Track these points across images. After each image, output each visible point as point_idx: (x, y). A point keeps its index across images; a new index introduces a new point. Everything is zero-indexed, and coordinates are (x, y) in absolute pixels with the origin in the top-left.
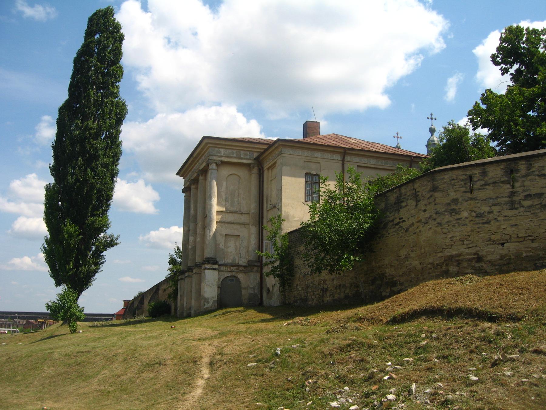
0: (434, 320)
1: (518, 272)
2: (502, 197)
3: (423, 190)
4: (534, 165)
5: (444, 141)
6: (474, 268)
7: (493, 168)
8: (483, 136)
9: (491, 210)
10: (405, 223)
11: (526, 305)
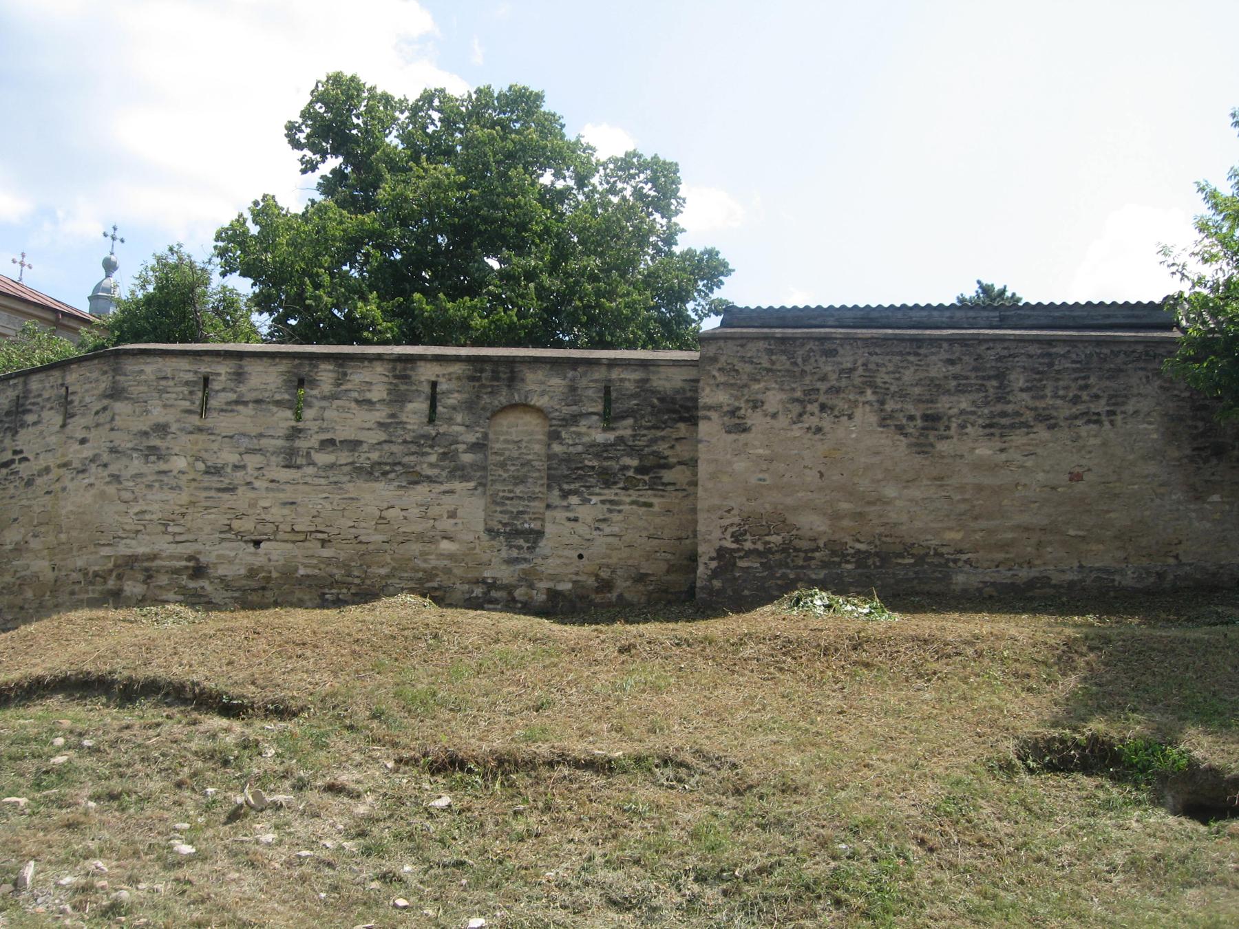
0: (86, 705)
1: (289, 609)
2: (272, 437)
3: (87, 391)
4: (352, 377)
5: (151, 289)
6: (183, 590)
7: (260, 369)
8: (238, 295)
9: (242, 463)
10: (27, 463)
11: (310, 683)
